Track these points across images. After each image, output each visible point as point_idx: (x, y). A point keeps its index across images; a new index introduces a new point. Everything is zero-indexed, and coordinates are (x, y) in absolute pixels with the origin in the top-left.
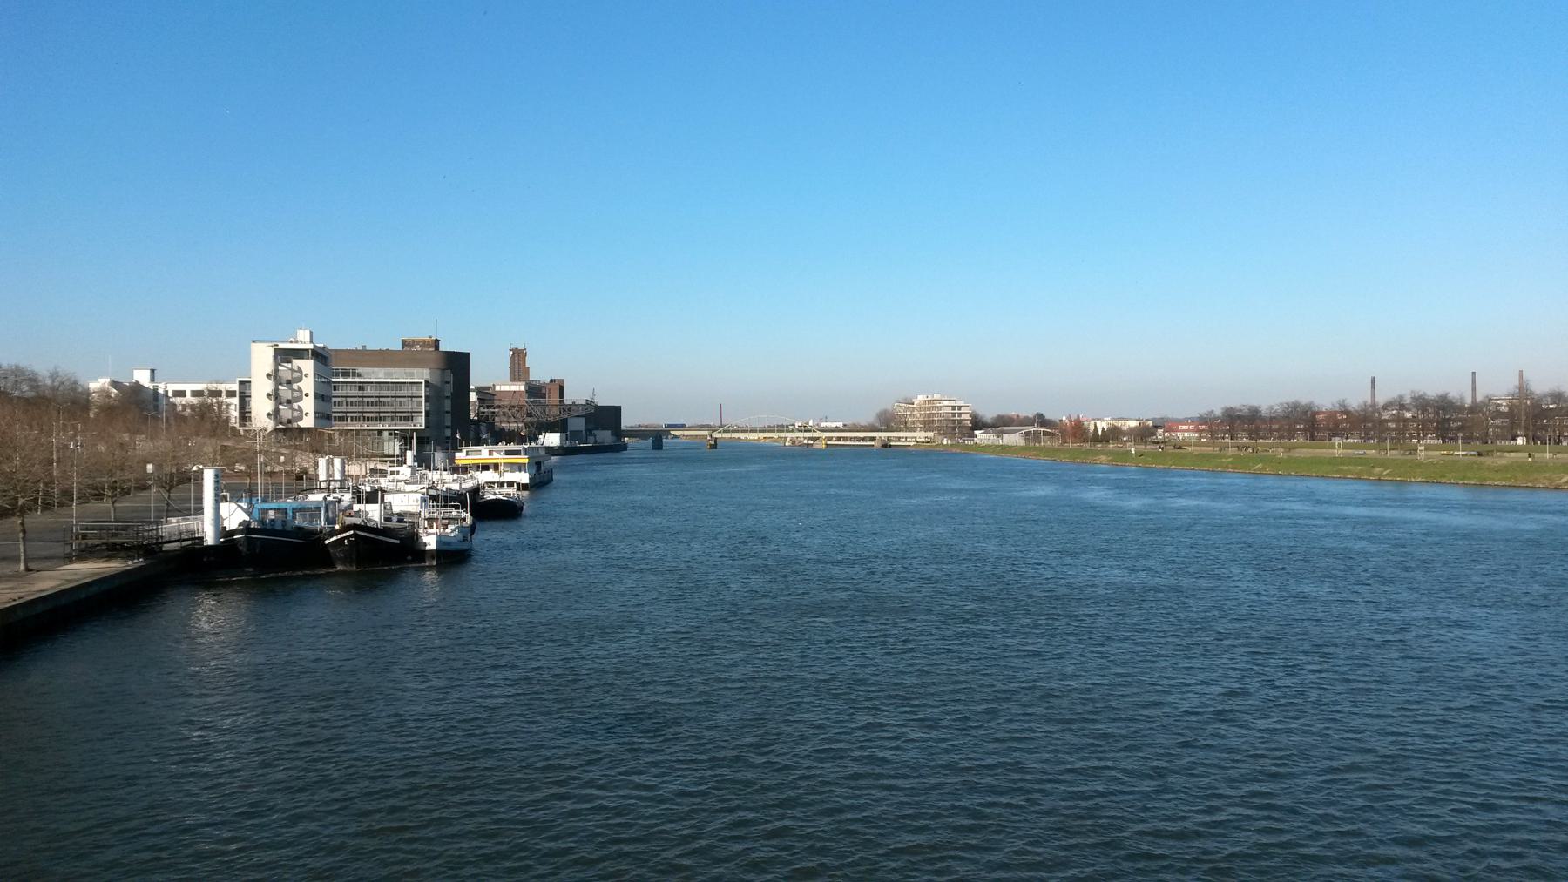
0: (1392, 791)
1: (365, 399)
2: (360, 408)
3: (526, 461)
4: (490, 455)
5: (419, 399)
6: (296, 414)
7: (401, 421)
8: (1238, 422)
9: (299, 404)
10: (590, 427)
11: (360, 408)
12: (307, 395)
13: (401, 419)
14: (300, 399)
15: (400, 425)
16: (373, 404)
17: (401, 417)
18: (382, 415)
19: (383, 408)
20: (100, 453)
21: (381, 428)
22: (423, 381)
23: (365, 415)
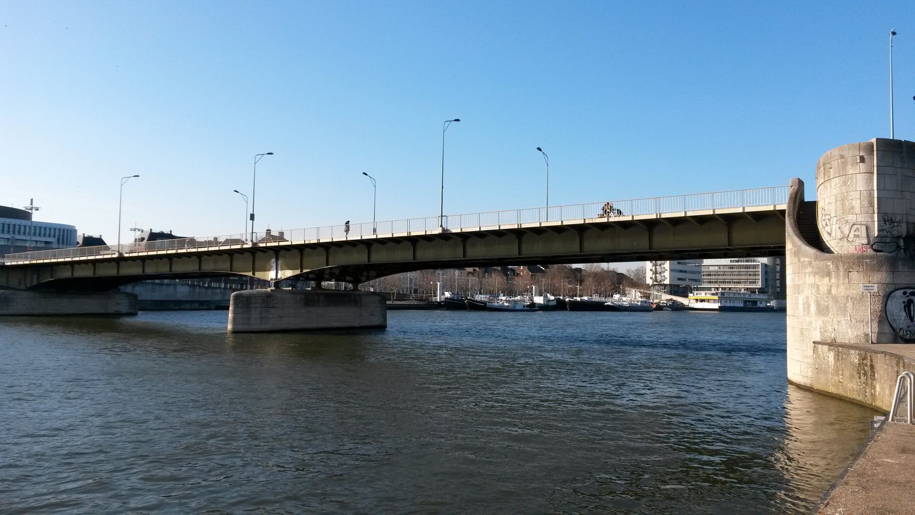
0: (678, 353)
1: (733, 273)
2: (731, 277)
3: (717, 298)
4: (706, 295)
5: (758, 273)
6: (663, 278)
7: (750, 283)
8: (818, 360)
9: (664, 274)
10: (766, 288)
11: (731, 277)
12: (667, 270)
13: (750, 282)
14: (664, 272)
15: (750, 285)
16: (738, 275)
17: (750, 282)
18: (741, 280)
19: (741, 277)
20: (176, 282)
21: (730, 287)
22: (760, 264)
23: (733, 280)
